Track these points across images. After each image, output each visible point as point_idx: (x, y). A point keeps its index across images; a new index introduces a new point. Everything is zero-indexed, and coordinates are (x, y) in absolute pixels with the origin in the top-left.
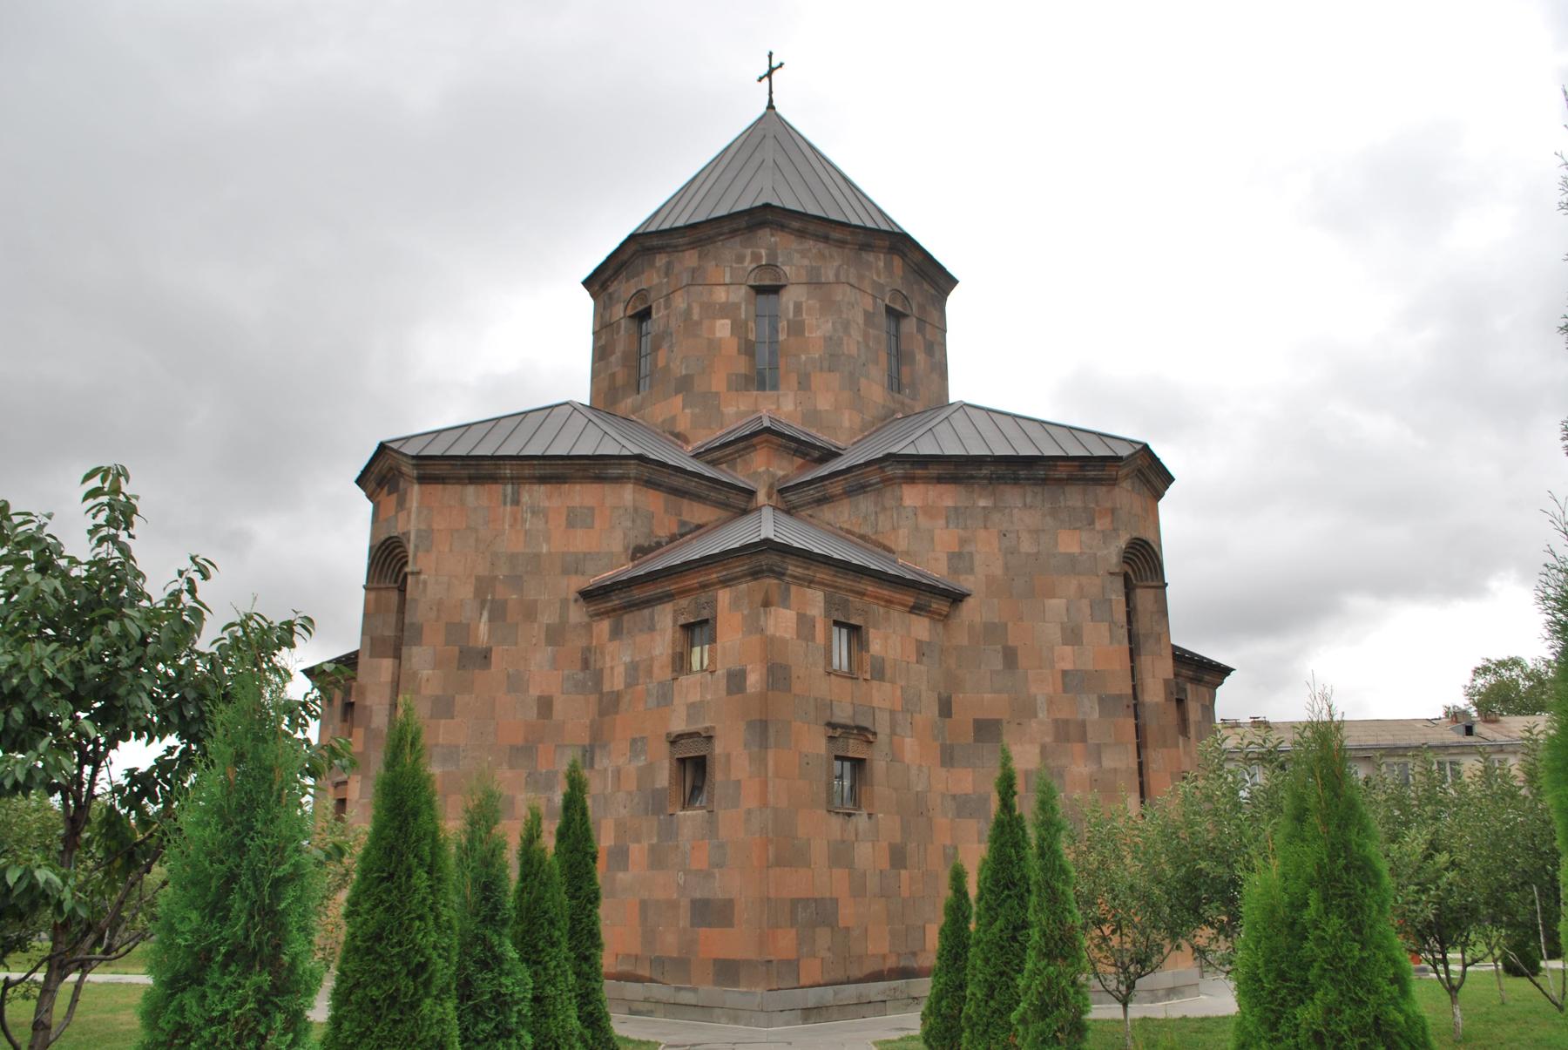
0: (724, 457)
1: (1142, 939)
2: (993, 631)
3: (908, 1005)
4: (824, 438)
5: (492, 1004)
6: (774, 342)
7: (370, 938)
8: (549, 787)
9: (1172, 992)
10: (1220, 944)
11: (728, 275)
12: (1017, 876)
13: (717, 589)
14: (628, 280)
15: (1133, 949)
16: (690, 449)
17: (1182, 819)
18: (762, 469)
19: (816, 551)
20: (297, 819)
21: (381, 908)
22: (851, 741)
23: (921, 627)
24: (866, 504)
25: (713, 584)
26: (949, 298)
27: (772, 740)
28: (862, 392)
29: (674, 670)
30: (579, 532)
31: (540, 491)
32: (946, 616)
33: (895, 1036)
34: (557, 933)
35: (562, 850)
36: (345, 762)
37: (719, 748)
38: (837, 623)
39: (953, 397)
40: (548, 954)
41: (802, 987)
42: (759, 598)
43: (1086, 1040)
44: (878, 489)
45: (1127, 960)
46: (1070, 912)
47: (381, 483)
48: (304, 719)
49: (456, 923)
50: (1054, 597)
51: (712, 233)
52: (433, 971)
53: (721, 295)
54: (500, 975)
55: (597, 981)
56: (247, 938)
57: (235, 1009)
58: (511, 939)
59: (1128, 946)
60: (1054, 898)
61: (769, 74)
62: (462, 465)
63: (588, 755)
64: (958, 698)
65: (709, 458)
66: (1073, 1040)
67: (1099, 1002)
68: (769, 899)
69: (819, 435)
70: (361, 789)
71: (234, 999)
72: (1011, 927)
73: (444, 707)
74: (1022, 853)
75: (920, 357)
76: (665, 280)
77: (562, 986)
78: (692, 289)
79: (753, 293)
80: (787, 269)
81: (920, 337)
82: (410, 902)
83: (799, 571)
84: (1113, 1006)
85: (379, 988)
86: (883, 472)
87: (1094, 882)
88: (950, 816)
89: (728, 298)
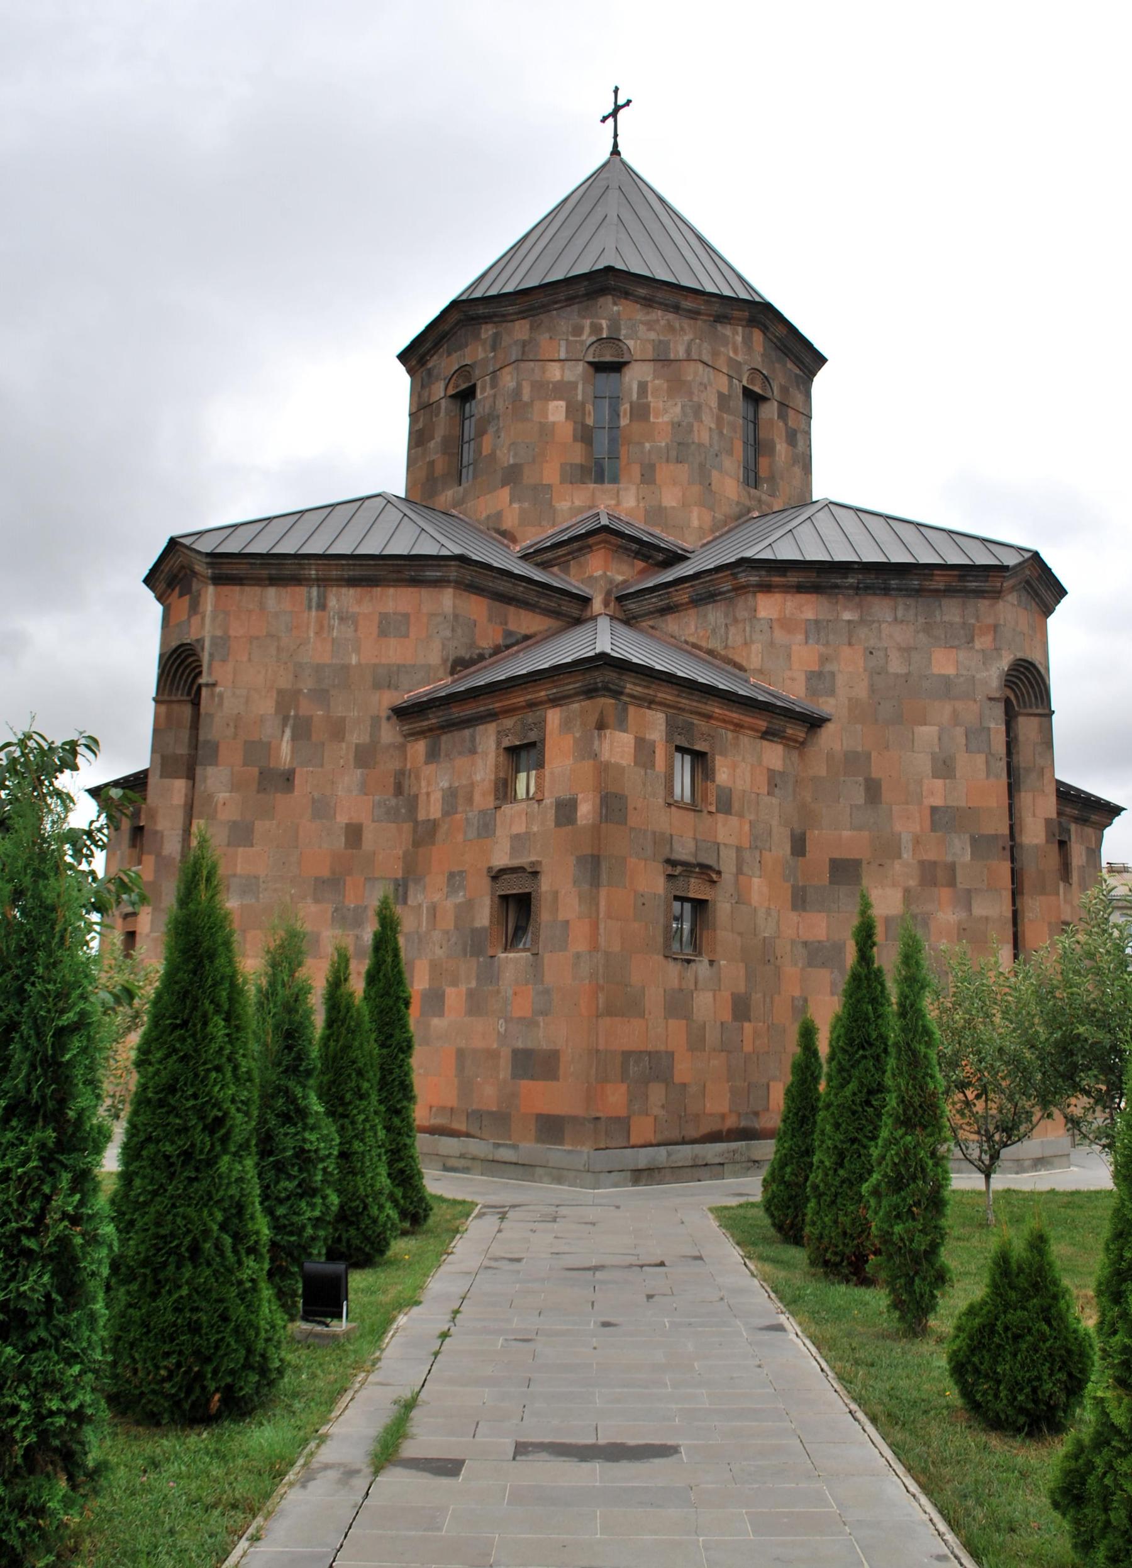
0: (555, 559)
1: (1009, 1106)
2: (854, 761)
3: (749, 1169)
4: (670, 539)
5: (295, 1161)
6: (614, 428)
7: (163, 1090)
8: (358, 923)
9: (1040, 1162)
10: (1097, 1114)
11: (563, 350)
12: (874, 1035)
13: (546, 709)
14: (449, 354)
15: (999, 1116)
16: (518, 548)
17: (1060, 978)
18: (600, 573)
19: (658, 667)
20: (82, 963)
21: (175, 1058)
22: (693, 880)
23: (774, 755)
24: (715, 615)
25: (541, 703)
26: (815, 379)
27: (604, 877)
28: (713, 487)
29: (497, 799)
30: (393, 642)
31: (349, 595)
32: (803, 743)
33: (733, 1202)
34: (366, 1085)
35: (372, 994)
36: (134, 897)
37: (545, 885)
38: (679, 749)
39: (818, 493)
40: (356, 1107)
41: (633, 1147)
42: (593, 719)
43: (944, 1216)
44: (731, 598)
45: (991, 1128)
46: (932, 1077)
47: (172, 583)
48: (89, 849)
49: (256, 1074)
50: (925, 724)
51: (545, 300)
52: (232, 1126)
53: (555, 373)
54: (304, 1129)
55: (409, 1136)
56: (29, 1091)
57: (18, 1167)
58: (316, 1092)
59: (994, 1112)
60: (915, 1063)
61: (614, 114)
62: (262, 564)
63: (400, 889)
64: (813, 835)
65: (539, 559)
66: (930, 1216)
67: (959, 1171)
68: (598, 1051)
69: (663, 535)
70: (152, 922)
71: (16, 1156)
72: (865, 1090)
73: (242, 834)
74: (881, 1010)
75: (781, 447)
76: (492, 354)
77: (370, 1141)
78: (522, 365)
79: (591, 370)
80: (630, 343)
81: (781, 424)
82: (206, 1052)
83: (639, 690)
84: (973, 1175)
85: (173, 1143)
86: (736, 579)
87: (959, 1043)
88: (800, 965)
89: (562, 376)
